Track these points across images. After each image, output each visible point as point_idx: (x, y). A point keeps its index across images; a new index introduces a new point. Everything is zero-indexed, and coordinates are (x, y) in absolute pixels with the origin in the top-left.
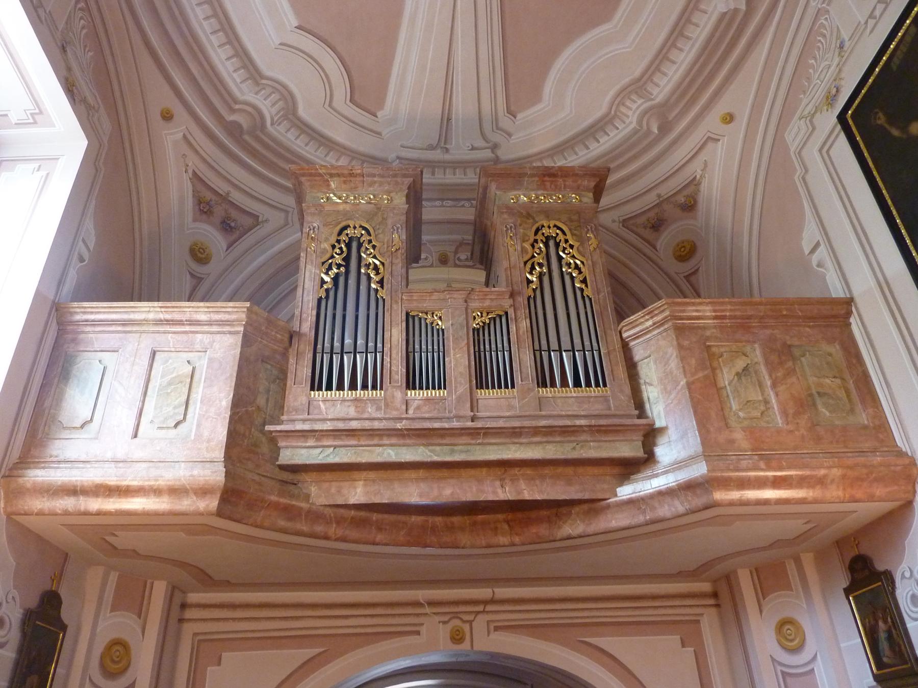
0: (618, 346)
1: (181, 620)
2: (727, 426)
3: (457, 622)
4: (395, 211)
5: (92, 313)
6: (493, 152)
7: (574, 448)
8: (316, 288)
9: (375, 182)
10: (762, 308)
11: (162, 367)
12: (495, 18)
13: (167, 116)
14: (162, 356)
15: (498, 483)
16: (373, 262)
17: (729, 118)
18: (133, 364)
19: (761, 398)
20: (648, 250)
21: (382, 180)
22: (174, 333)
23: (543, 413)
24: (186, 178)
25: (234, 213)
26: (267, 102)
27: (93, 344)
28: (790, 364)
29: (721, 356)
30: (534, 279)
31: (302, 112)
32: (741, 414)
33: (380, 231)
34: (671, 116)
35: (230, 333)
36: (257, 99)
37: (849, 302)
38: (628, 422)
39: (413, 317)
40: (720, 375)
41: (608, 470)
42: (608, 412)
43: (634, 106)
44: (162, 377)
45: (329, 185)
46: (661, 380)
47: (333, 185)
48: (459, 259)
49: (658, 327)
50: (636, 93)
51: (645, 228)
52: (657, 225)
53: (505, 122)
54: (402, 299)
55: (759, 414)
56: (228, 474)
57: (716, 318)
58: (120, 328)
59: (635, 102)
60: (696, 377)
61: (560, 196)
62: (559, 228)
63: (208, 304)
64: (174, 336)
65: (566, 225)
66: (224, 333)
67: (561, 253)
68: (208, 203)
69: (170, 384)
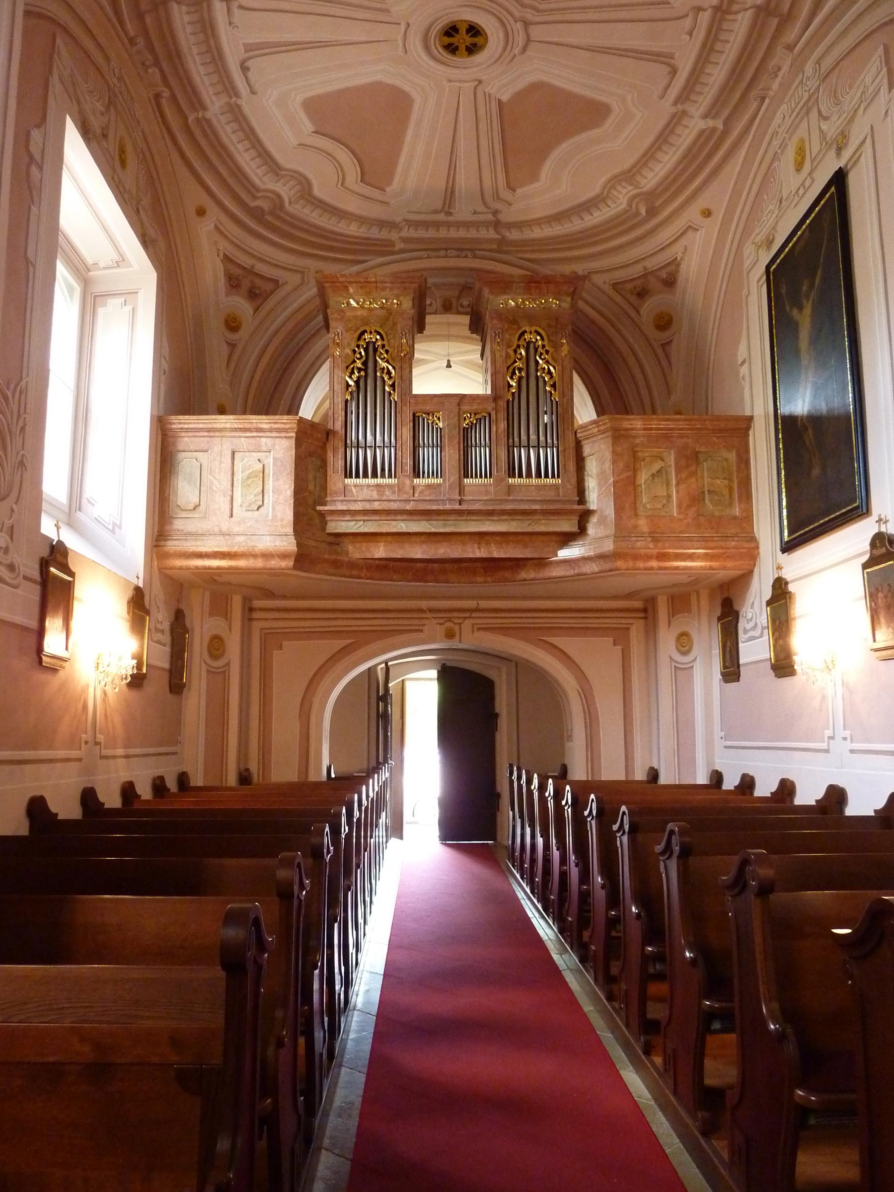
0: (572, 444)
1: (250, 620)
2: (636, 515)
3: (449, 624)
5: (185, 423)
7: (530, 525)
9: (387, 287)
12: (495, 123)
15: (476, 546)
16: (387, 367)
17: (707, 213)
18: (220, 463)
19: (665, 494)
20: (633, 314)
22: (245, 437)
23: (510, 498)
25: (258, 282)
28: (693, 468)
29: (644, 460)
30: (514, 384)
31: (316, 192)
32: (648, 506)
33: (392, 336)
35: (286, 437)
37: (750, 419)
38: (569, 507)
40: (640, 475)
41: (554, 538)
42: (557, 498)
43: (624, 191)
44: (243, 472)
45: (348, 290)
46: (598, 475)
47: (351, 290)
48: (461, 305)
49: (602, 434)
51: (632, 293)
52: (642, 294)
53: (505, 194)
55: (661, 506)
56: (298, 545)
57: (645, 429)
58: (206, 434)
59: (625, 188)
61: (543, 301)
62: (539, 334)
63: (269, 417)
64: (245, 439)
67: (538, 358)
68: (237, 279)
69: (248, 478)
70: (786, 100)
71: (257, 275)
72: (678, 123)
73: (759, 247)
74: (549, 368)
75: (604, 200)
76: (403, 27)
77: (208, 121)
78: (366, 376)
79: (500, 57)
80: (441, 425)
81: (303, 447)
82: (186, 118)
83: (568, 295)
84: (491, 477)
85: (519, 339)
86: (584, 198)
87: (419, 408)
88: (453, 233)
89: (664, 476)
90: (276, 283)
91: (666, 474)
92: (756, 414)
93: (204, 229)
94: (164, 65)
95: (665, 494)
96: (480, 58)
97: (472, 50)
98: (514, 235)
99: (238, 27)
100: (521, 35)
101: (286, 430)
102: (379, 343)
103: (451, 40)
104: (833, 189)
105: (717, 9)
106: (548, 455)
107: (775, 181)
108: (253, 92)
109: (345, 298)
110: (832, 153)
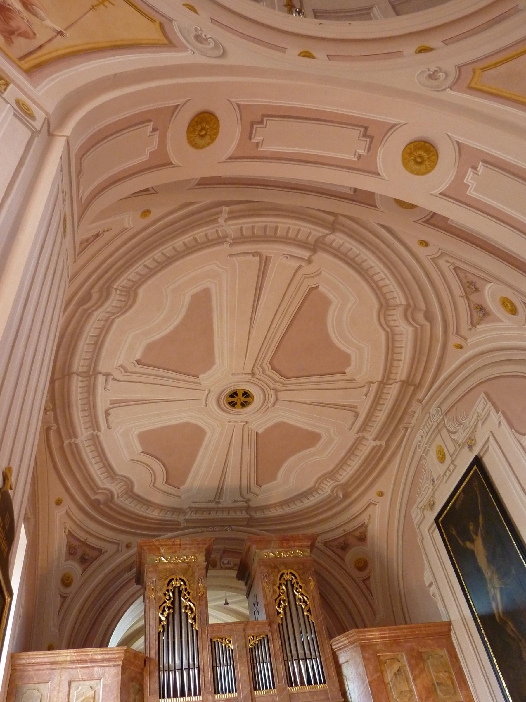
0: (330, 655)
4: (199, 567)
6: (246, 503)
8: (157, 625)
9: (186, 548)
10: (405, 631)
11: (76, 692)
13: (59, 503)
14: (75, 684)
16: (190, 605)
19: (408, 689)
20: (338, 560)
21: (191, 546)
22: (81, 668)
24: (64, 535)
25: (88, 550)
26: (117, 487)
27: (33, 679)
28: (422, 665)
29: (386, 662)
30: (282, 612)
31: (136, 490)
33: (192, 582)
34: (350, 490)
36: (112, 486)
37: (449, 624)
39: (215, 642)
43: (329, 484)
45: (160, 551)
47: (162, 551)
48: (224, 564)
49: (351, 644)
50: (330, 478)
52: (345, 547)
53: (255, 489)
54: (207, 630)
57: (382, 638)
59: (329, 482)
60: (374, 678)
61: (292, 552)
62: (293, 575)
64: (81, 670)
65: (296, 572)
66: (110, 666)
67: (295, 591)
68: (74, 548)
70: (421, 428)
71: (88, 546)
72: (360, 443)
73: (424, 509)
74: (304, 599)
75: (316, 490)
76: (207, 392)
77: (76, 445)
78: (173, 613)
79: (260, 409)
80: (232, 647)
81: (127, 673)
82: (63, 443)
83: (307, 547)
84: (274, 687)
85: (280, 579)
86: (304, 489)
87: (214, 635)
88: (220, 515)
89: (403, 674)
90: (100, 552)
91: (404, 672)
92: (453, 619)
93: (59, 513)
94: (58, 411)
95: (408, 689)
96: (247, 409)
97: (243, 405)
98: (258, 515)
99: (109, 390)
100: (273, 397)
101: (114, 660)
102: (183, 587)
103: (233, 399)
104: (475, 467)
105: (381, 382)
106: (314, 665)
107: (425, 470)
108: (109, 428)
109: (158, 556)
110: (466, 449)
